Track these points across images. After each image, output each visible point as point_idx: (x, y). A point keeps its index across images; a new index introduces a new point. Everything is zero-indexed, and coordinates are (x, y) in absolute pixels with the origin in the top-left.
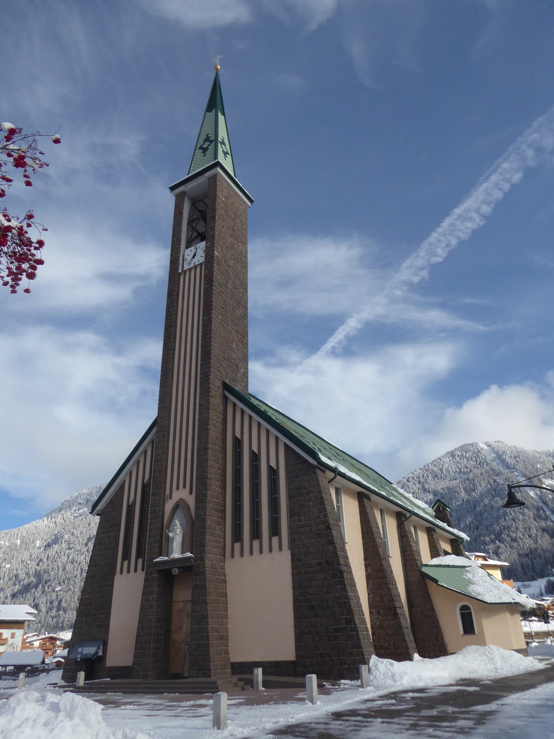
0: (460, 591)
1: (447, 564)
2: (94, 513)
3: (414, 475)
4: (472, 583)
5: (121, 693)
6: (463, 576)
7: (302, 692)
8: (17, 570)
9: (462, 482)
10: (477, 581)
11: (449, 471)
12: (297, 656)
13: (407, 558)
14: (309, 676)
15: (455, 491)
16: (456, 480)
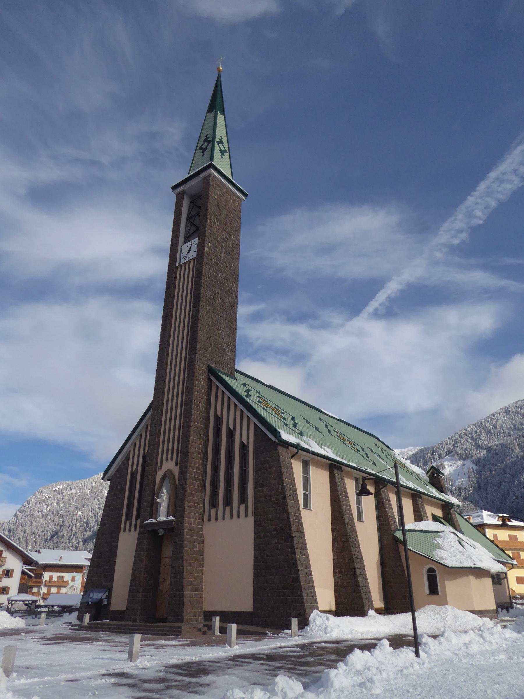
0: (425, 555)
1: (421, 529)
2: (105, 478)
3: (466, 431)
4: (440, 548)
5: (110, 633)
6: (433, 541)
7: (241, 638)
8: (88, 518)
9: (516, 438)
10: (444, 545)
11: (503, 427)
12: (254, 608)
13: (383, 522)
14: (230, 625)
15: (509, 448)
16: (510, 436)
